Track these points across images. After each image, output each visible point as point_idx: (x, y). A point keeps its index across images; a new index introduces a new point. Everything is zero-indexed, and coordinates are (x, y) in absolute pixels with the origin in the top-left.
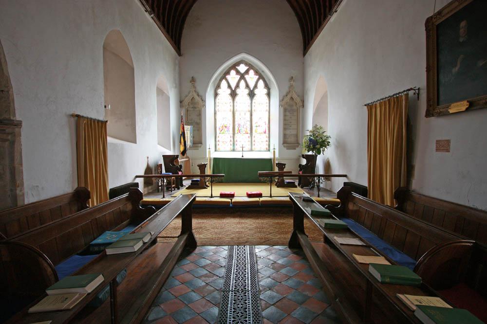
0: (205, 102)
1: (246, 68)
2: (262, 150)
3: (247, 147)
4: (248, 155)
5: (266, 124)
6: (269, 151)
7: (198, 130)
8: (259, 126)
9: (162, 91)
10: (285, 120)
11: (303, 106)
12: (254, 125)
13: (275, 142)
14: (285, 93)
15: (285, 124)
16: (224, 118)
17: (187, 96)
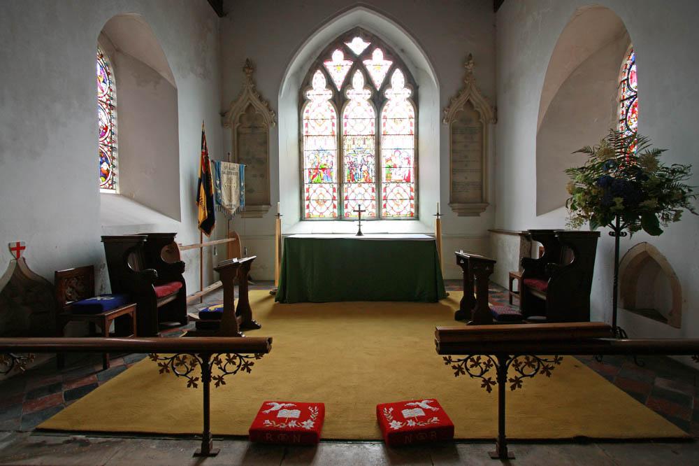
0: (276, 113)
1: (366, 45)
2: (402, 216)
3: (370, 209)
4: (373, 230)
5: (409, 163)
6: (417, 218)
7: (262, 176)
8: (395, 167)
9: (156, 72)
10: (453, 151)
11: (496, 119)
12: (384, 163)
13: (431, 201)
14: (453, 92)
15: (453, 161)
16: (320, 147)
17: (235, 101)
